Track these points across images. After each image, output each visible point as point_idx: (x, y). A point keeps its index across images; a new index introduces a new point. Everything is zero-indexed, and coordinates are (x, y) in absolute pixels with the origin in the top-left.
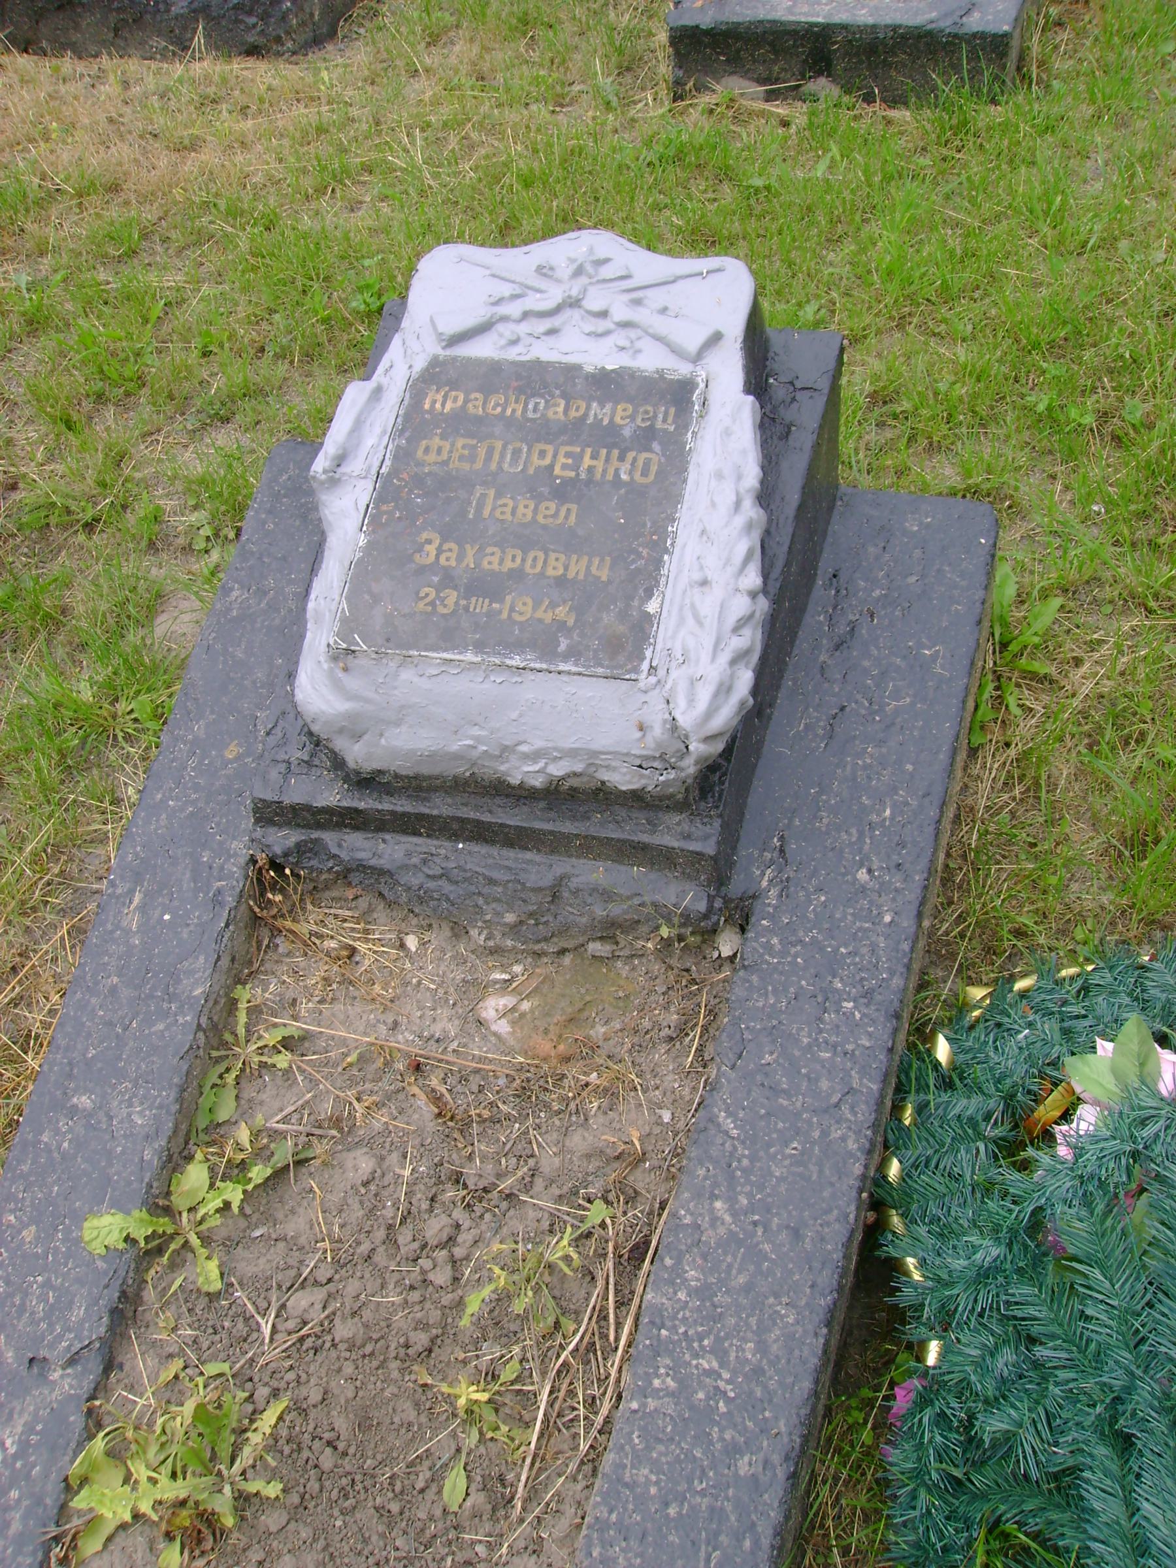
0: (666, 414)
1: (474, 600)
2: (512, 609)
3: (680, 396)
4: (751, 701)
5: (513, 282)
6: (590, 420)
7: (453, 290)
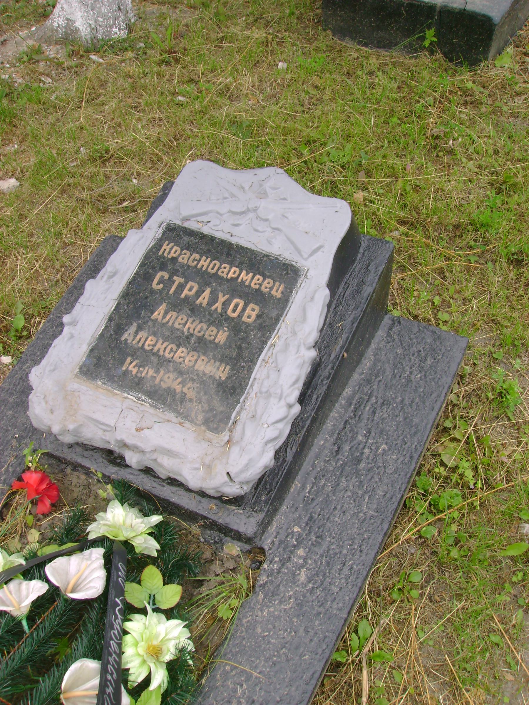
6: (239, 280)
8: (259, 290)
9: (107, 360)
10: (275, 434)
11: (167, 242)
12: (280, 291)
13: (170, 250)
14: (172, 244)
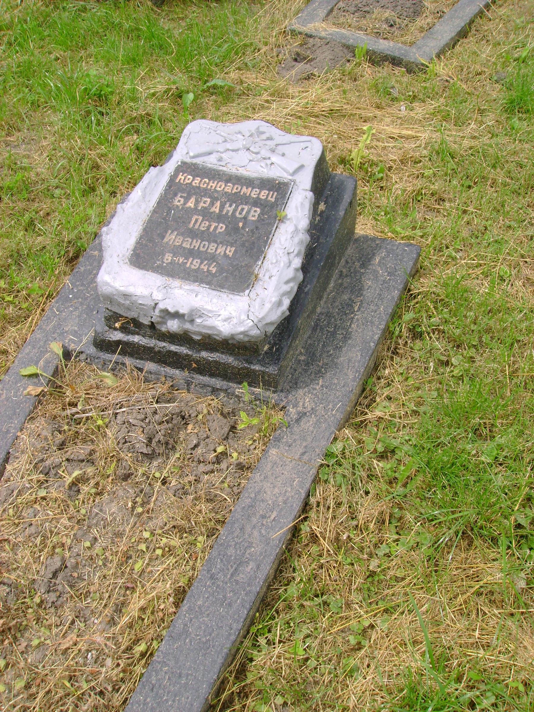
0: (273, 194)
2: (191, 263)
3: (281, 189)
4: (288, 313)
6: (242, 194)
7: (201, 140)
8: (258, 198)
9: (144, 257)
12: (274, 196)
13: (184, 178)
14: (185, 175)
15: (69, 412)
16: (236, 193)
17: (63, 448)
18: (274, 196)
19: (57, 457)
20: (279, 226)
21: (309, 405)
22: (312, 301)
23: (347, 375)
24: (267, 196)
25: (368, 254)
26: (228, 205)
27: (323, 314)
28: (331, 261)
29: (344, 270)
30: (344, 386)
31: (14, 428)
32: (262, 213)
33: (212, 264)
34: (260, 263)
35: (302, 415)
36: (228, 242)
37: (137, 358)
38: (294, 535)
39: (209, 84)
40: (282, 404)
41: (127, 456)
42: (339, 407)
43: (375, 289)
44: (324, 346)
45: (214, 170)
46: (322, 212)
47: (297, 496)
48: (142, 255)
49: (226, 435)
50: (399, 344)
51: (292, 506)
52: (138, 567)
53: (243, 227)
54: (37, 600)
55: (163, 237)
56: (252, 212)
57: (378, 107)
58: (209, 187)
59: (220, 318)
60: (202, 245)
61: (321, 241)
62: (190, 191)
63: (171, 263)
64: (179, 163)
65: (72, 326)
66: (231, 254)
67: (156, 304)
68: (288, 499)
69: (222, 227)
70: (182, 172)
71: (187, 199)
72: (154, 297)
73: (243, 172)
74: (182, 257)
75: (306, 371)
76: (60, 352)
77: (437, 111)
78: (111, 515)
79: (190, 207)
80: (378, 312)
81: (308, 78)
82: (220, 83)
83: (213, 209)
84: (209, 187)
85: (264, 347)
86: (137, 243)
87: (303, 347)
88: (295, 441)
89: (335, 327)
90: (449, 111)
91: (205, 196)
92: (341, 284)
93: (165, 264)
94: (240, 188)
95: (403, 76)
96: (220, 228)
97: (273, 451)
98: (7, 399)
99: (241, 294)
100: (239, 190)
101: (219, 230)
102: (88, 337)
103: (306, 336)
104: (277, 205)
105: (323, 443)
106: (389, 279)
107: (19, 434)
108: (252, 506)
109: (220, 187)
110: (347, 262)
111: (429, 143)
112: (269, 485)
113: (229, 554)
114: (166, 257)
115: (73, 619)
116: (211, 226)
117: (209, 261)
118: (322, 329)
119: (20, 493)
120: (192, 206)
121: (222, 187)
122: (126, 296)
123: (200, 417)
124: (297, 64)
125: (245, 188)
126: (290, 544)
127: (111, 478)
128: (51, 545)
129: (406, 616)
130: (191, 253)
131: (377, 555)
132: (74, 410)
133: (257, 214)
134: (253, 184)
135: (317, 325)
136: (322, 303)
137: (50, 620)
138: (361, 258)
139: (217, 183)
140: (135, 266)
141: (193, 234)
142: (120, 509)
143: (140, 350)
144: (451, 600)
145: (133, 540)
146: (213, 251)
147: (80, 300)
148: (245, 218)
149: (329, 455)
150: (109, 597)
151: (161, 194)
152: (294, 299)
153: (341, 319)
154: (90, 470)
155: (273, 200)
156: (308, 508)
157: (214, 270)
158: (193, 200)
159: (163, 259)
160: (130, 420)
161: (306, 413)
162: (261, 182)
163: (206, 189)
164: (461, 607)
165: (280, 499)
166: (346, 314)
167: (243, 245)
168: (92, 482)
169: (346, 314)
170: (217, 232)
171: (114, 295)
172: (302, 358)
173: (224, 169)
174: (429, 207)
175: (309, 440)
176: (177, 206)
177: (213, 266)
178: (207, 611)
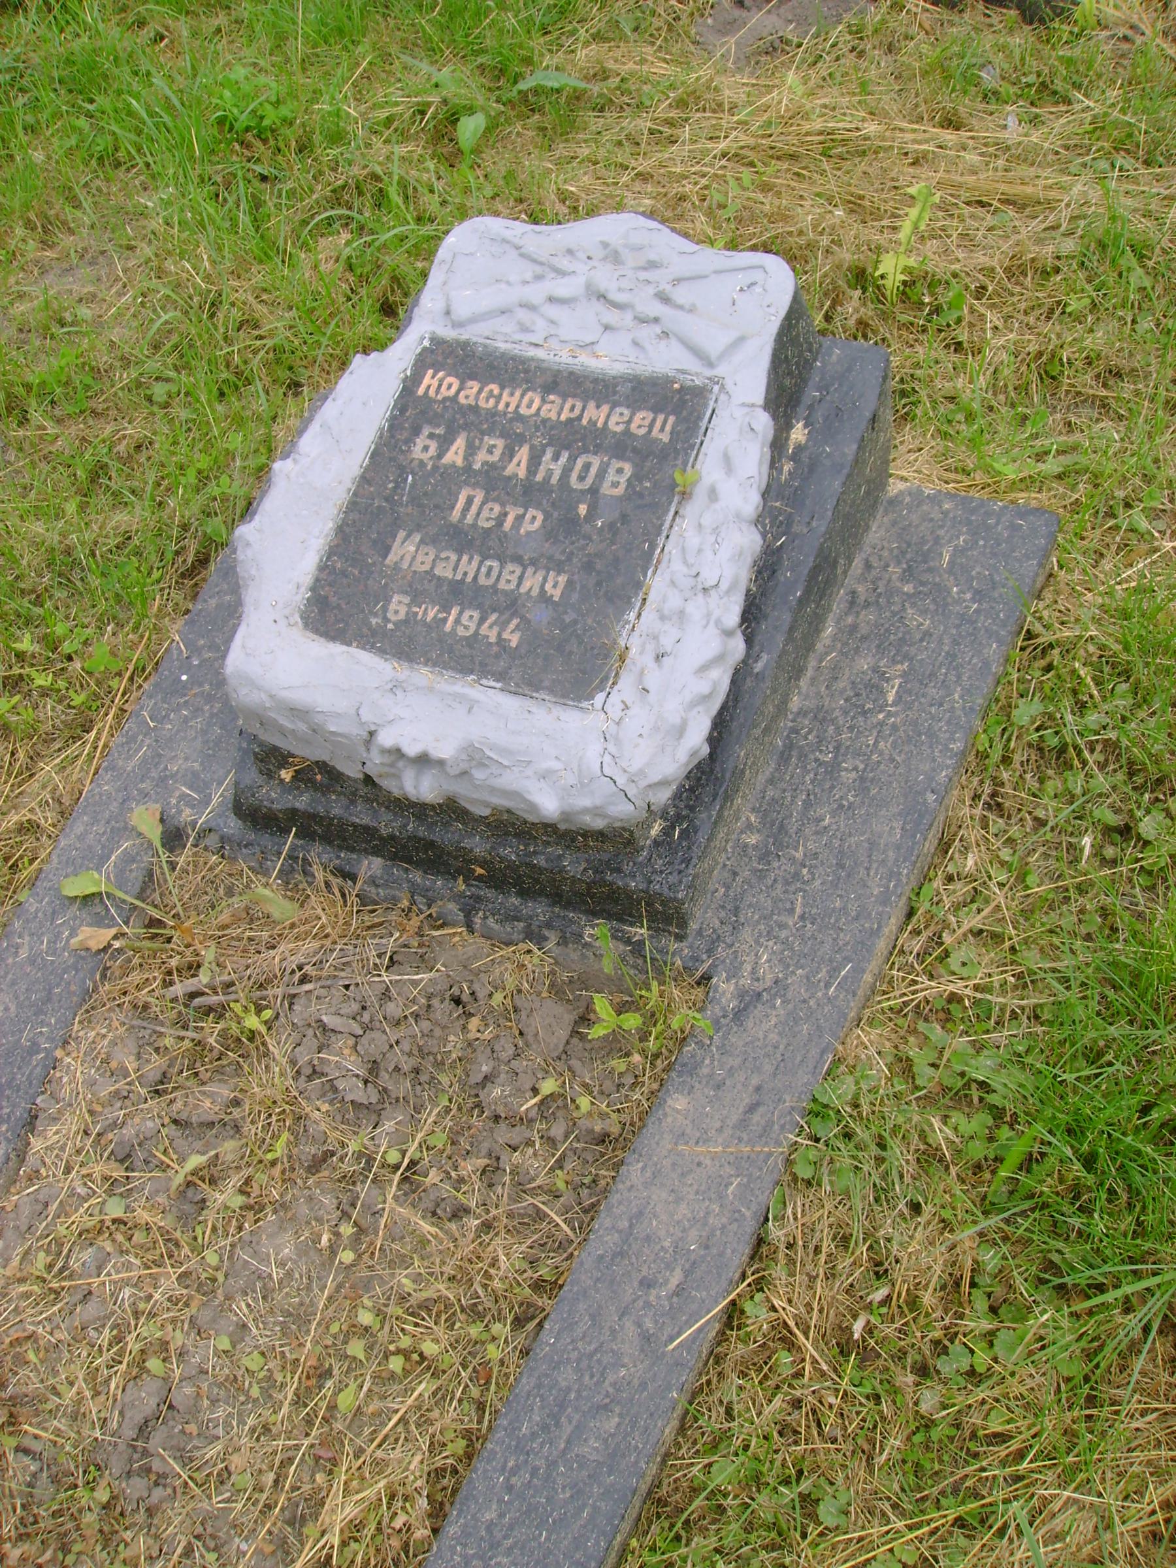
1: (455, 611)
2: (457, 621)
3: (684, 404)
4: (706, 750)
5: (535, 261)
6: (584, 422)
8: (627, 432)
9: (338, 606)
10: (704, 687)
11: (430, 372)
12: (668, 428)
15: (179, 989)
16: (570, 421)
17: (165, 1091)
18: (668, 428)
19: (148, 1118)
20: (681, 512)
21: (768, 972)
22: (774, 691)
23: (865, 886)
24: (651, 426)
25: (923, 541)
26: (548, 455)
27: (805, 714)
28: (822, 578)
29: (860, 589)
30: (857, 918)
31: (50, 1039)
32: (637, 477)
33: (508, 622)
34: (632, 616)
35: (749, 1000)
36: (550, 558)
37: (340, 848)
38: (729, 1325)
39: (523, 86)
40: (702, 969)
41: (319, 1112)
42: (845, 977)
43: (940, 642)
44: (807, 804)
45: (513, 358)
46: (799, 448)
47: (735, 1226)
48: (334, 600)
49: (561, 1048)
50: (1002, 784)
51: (721, 1254)
52: (346, 1400)
53: (591, 516)
54: (103, 1495)
55: (387, 550)
56: (611, 471)
57: (951, 122)
58: (501, 407)
59: (529, 772)
60: (484, 570)
61: (796, 528)
62: (454, 420)
63: (406, 622)
64: (426, 343)
65: (186, 759)
66: (557, 594)
67: (372, 734)
68: (712, 1234)
69: (534, 518)
70: (432, 366)
71: (445, 443)
72: (366, 716)
73: (587, 362)
74: (434, 603)
75: (760, 875)
76: (154, 833)
77: (1099, 127)
78: (281, 1264)
79: (453, 465)
80: (946, 706)
81: (771, 51)
82: (552, 81)
83: (510, 469)
84: (501, 407)
85: (650, 827)
86: (322, 568)
87: (753, 810)
88: (731, 1071)
89: (837, 748)
90: (1130, 124)
91: (490, 432)
92: (854, 628)
93: (390, 626)
94: (579, 405)
95: (1011, 31)
96: (527, 518)
97: (677, 1102)
98: (32, 960)
99: (585, 704)
100: (577, 412)
101: (527, 527)
102: (220, 795)
103: (761, 779)
104: (677, 452)
105: (803, 1077)
106: (977, 611)
107: (59, 1053)
108: (622, 1254)
109: (530, 404)
110: (868, 566)
111: (1077, 217)
112: (664, 1195)
113: (564, 1384)
114: (393, 606)
115: (190, 1543)
116: (506, 514)
117: (501, 613)
118: (803, 756)
119: (63, 1212)
120: (459, 462)
121: (535, 406)
122: (298, 712)
123: (498, 997)
124: (745, 14)
125: (592, 405)
126: (719, 1344)
127: (279, 1166)
128: (138, 1347)
129: (1011, 1540)
130: (457, 593)
131: (938, 1372)
132: (191, 984)
133: (623, 480)
134: (615, 393)
135: (789, 746)
136: (804, 683)
137: (134, 1546)
138: (903, 553)
139: (522, 396)
140: (316, 631)
141: (462, 539)
142: (302, 1251)
143: (346, 830)
144: (1126, 1498)
145: (334, 1328)
146: (512, 586)
147: (207, 687)
148: (594, 491)
149: (818, 1111)
150: (276, 1482)
151: (381, 429)
152: (724, 708)
153: (851, 729)
154: (229, 1148)
155: (665, 437)
156: (764, 1250)
157: (514, 640)
158: (460, 443)
159: (385, 609)
160: (324, 1018)
161: (759, 995)
162: (634, 389)
163: (493, 413)
164: (1153, 1518)
165: (693, 1234)
166: (865, 713)
167: (588, 567)
168: (235, 1180)
169: (865, 713)
170: (522, 531)
171: (266, 708)
172: (753, 839)
173: (540, 354)
174: (1078, 393)
175: (768, 1068)
176: (421, 461)
177: (512, 626)
178: (505, 1537)
